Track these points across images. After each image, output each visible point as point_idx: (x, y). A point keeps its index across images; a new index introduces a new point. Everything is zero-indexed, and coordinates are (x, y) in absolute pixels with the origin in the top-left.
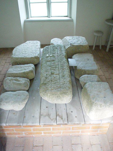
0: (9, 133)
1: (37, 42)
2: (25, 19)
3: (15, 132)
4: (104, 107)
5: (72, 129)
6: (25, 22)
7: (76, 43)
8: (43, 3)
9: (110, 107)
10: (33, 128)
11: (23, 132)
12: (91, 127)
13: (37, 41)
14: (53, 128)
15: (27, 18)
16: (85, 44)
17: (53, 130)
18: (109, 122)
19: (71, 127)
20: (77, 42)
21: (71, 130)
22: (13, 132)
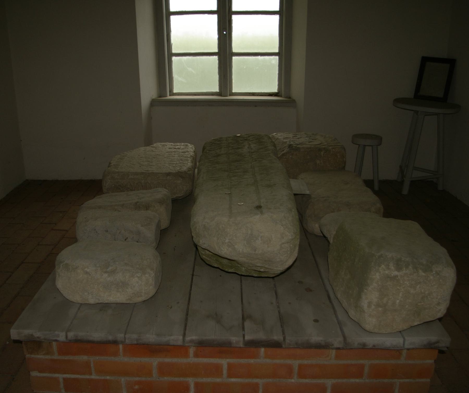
0: (74, 379)
1: (187, 145)
2: (154, 98)
3: (93, 377)
4: (410, 267)
5: (301, 376)
6: (153, 103)
7: (307, 143)
8: (206, 15)
9: (432, 271)
10: (161, 360)
11: (123, 380)
12: (366, 370)
13: (187, 144)
14: (230, 365)
15: (160, 97)
16: (332, 146)
17: (230, 376)
18: (430, 346)
19: (295, 363)
20: (309, 142)
21: (295, 363)
22: (88, 377)
